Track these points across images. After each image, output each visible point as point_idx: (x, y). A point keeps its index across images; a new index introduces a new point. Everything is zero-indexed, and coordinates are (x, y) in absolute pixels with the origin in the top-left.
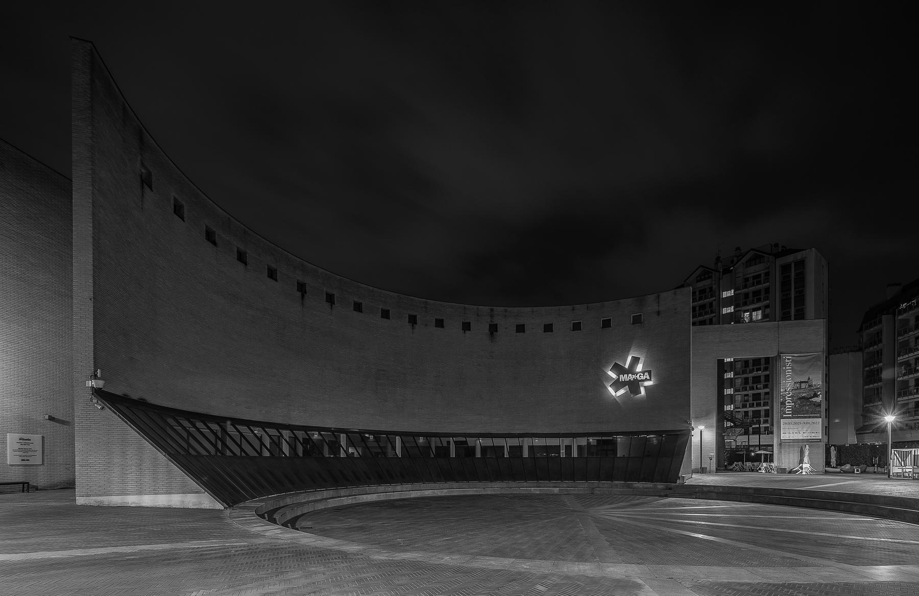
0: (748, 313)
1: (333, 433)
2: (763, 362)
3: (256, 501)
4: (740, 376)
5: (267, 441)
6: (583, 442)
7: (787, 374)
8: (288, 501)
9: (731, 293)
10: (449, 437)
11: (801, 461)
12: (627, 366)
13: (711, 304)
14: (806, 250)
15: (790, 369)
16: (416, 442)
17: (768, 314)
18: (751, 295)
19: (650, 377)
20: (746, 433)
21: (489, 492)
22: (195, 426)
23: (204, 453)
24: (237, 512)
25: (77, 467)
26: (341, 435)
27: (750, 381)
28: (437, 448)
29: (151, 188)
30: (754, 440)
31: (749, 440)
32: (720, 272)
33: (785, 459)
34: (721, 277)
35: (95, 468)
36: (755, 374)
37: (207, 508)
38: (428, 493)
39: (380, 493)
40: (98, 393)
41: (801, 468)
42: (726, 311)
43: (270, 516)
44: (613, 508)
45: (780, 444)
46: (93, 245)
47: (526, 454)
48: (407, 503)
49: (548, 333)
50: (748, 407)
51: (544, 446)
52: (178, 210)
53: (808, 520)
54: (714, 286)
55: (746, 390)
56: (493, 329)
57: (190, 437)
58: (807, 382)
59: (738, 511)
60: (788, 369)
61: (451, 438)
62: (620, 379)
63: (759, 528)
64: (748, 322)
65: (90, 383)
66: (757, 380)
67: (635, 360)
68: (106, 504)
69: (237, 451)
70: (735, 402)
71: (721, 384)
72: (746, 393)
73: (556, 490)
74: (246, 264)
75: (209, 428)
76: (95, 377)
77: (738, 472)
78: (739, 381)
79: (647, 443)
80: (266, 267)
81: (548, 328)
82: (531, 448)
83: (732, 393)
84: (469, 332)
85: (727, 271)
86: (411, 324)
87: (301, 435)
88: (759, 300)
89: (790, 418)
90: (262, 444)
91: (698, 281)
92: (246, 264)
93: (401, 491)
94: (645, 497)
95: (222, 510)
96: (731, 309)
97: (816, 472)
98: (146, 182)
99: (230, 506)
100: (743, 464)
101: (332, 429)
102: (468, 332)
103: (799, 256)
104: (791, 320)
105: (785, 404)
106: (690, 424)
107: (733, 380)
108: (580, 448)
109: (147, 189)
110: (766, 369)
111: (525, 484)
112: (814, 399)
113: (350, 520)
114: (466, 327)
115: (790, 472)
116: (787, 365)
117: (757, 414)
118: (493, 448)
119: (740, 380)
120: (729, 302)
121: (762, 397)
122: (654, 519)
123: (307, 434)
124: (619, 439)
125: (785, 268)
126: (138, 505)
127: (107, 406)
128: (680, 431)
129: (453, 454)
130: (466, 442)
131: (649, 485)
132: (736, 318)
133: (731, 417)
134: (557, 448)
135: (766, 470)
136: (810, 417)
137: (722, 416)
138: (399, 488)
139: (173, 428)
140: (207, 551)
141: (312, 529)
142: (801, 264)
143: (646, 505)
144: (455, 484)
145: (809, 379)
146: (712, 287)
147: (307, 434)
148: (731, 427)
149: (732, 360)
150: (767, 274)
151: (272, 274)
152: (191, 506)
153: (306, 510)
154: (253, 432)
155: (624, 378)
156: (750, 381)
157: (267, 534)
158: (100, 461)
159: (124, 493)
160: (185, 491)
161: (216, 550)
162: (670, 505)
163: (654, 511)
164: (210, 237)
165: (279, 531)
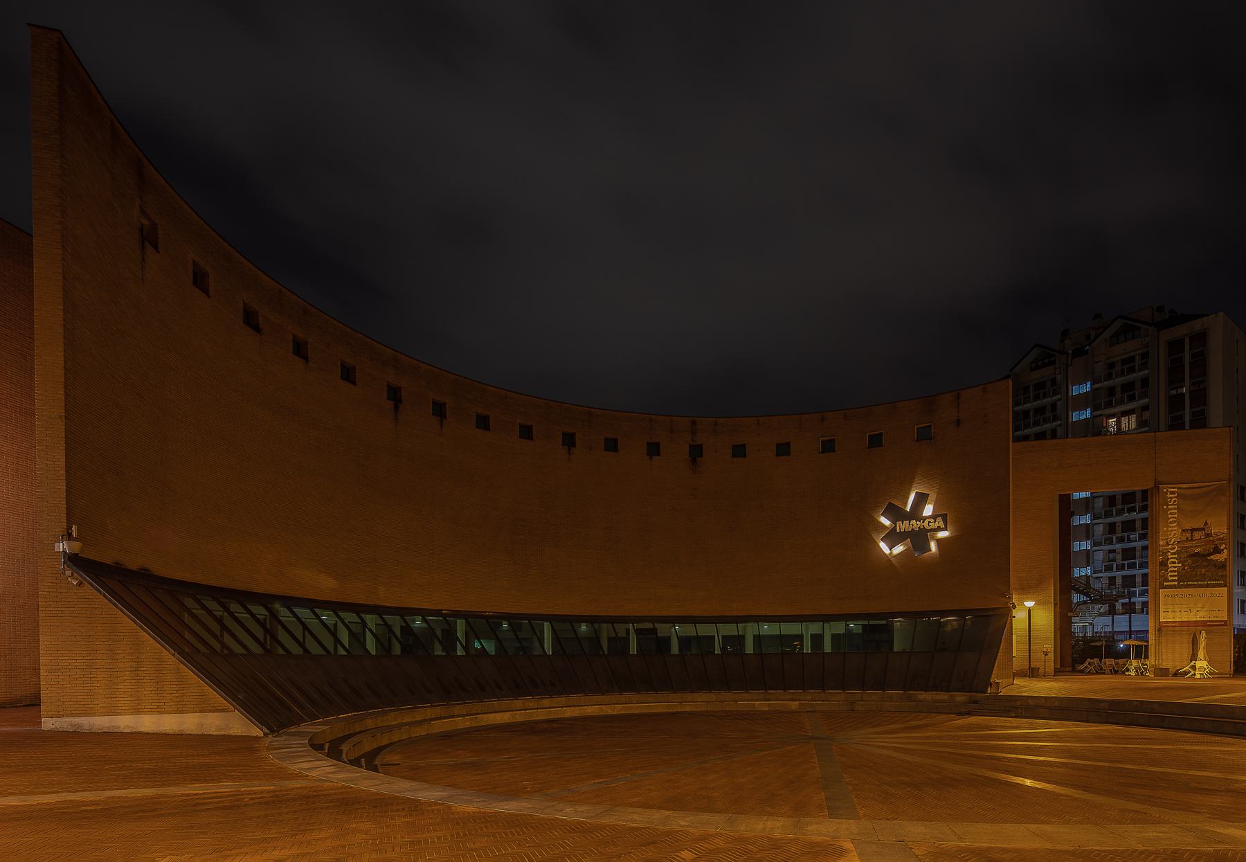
0: (1115, 420)
1: (445, 618)
2: (1139, 496)
3: (319, 724)
4: (1100, 521)
5: (345, 637)
6: (839, 628)
7: (1170, 516)
8: (370, 723)
9: (1087, 388)
10: (626, 623)
11: (1194, 657)
12: (908, 509)
13: (1054, 406)
14: (1208, 315)
15: (1175, 509)
16: (575, 632)
17: (1147, 420)
18: (1118, 390)
19: (946, 524)
20: (1112, 612)
21: (688, 708)
22: (204, 607)
23: (238, 649)
24: (282, 740)
25: (43, 673)
26: (458, 621)
27: (1119, 529)
28: (610, 639)
29: (156, 248)
30: (1121, 623)
31: (1113, 623)
32: (1068, 354)
33: (1167, 655)
34: (1070, 363)
35: (70, 674)
36: (1127, 516)
37: (239, 734)
38: (592, 710)
39: (515, 711)
40: (74, 560)
41: (1194, 668)
42: (1076, 416)
43: (334, 751)
44: (875, 733)
45: (1160, 630)
46: (65, 338)
47: (749, 648)
48: (555, 725)
49: (782, 458)
50: (1115, 570)
51: (777, 636)
52: (200, 280)
53: (1186, 751)
54: (1059, 377)
55: (1111, 543)
56: (696, 452)
57: (225, 634)
58: (1203, 529)
59: (1101, 738)
60: (1171, 509)
61: (631, 625)
62: (898, 528)
63: (1101, 764)
64: (1114, 434)
65: (61, 546)
66: (1129, 526)
67: (921, 500)
68: (86, 728)
69: (296, 650)
70: (1093, 563)
71: (1066, 534)
72: (1110, 547)
73: (794, 705)
74: (306, 359)
75: (249, 612)
76: (69, 537)
77: (1093, 674)
78: (1099, 530)
79: (941, 630)
80: (339, 363)
81: (783, 449)
82: (758, 639)
83: (1089, 548)
84: (657, 458)
85: (1079, 352)
86: (567, 447)
87: (395, 622)
88: (1132, 398)
89: (1174, 587)
90: (337, 641)
91: (1032, 370)
92: (306, 359)
93: (550, 708)
94: (933, 715)
95: (260, 737)
96: (1087, 414)
97: (1218, 674)
98: (148, 238)
99: (272, 731)
100: (1101, 662)
101: (443, 611)
102: (656, 458)
103: (1197, 325)
104: (1184, 429)
105: (1166, 565)
106: (1010, 598)
107: (1091, 528)
108: (835, 638)
109: (150, 249)
110: (1144, 508)
111: (746, 695)
112: (1214, 557)
113: (460, 752)
114: (654, 449)
115: (1176, 674)
116: (1175, 501)
117: (1129, 581)
118: (698, 638)
119: (1101, 527)
120: (1082, 402)
121: (1138, 554)
122: (935, 749)
123: (405, 621)
124: (898, 622)
125: (1175, 346)
126: (134, 730)
127: (88, 582)
128: (993, 609)
129: (633, 649)
130: (654, 631)
131: (943, 696)
132: (1093, 429)
133: (1085, 587)
134: (800, 637)
135: (1137, 671)
136: (1207, 586)
137: (1067, 585)
138: (546, 702)
139: (191, 611)
140: (208, 798)
141: (398, 766)
142: (1200, 338)
143: (931, 728)
144: (635, 697)
145: (1206, 524)
146: (1055, 378)
147: (405, 621)
148: (1085, 603)
149: (1089, 495)
150: (1145, 356)
151: (348, 374)
152: (214, 732)
153: (396, 737)
154: (318, 617)
155: (902, 526)
156: (1119, 529)
157: (313, 774)
158: (76, 664)
159: (112, 712)
160: (204, 707)
161: (221, 797)
162: (970, 727)
163: (941, 738)
164: (250, 319)
165: (332, 769)
